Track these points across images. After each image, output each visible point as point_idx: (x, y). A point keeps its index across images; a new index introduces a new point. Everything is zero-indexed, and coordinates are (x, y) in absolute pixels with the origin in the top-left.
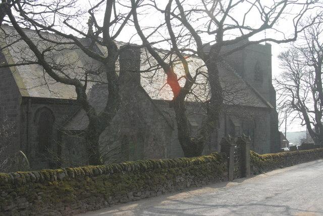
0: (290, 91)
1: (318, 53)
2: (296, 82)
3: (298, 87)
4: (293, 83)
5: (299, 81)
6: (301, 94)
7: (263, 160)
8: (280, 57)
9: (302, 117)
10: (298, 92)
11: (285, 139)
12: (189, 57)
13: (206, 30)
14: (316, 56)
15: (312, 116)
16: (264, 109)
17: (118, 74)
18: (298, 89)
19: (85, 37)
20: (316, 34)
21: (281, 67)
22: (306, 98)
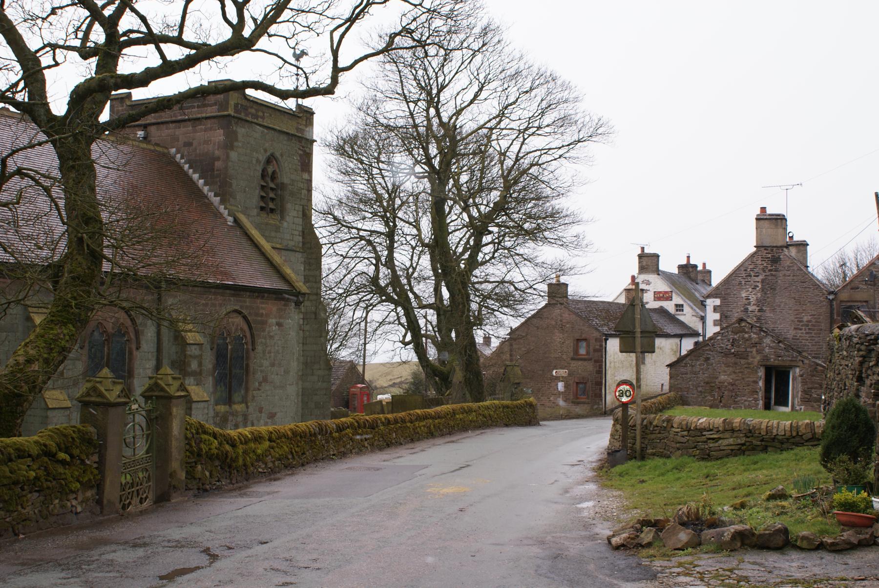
0: (369, 248)
1: (438, 142)
2: (387, 224)
3: (390, 235)
4: (379, 226)
5: (394, 222)
6: (402, 257)
7: (233, 446)
8: (340, 150)
9: (404, 320)
10: (391, 249)
11: (363, 381)
12: (534, 133)
13: (77, 43)
14: (433, 150)
15: (427, 319)
16: (275, 294)
17: (437, 168)
18: (392, 242)
19: (193, 52)
20: (435, 91)
21: (341, 177)
22: (414, 269)
